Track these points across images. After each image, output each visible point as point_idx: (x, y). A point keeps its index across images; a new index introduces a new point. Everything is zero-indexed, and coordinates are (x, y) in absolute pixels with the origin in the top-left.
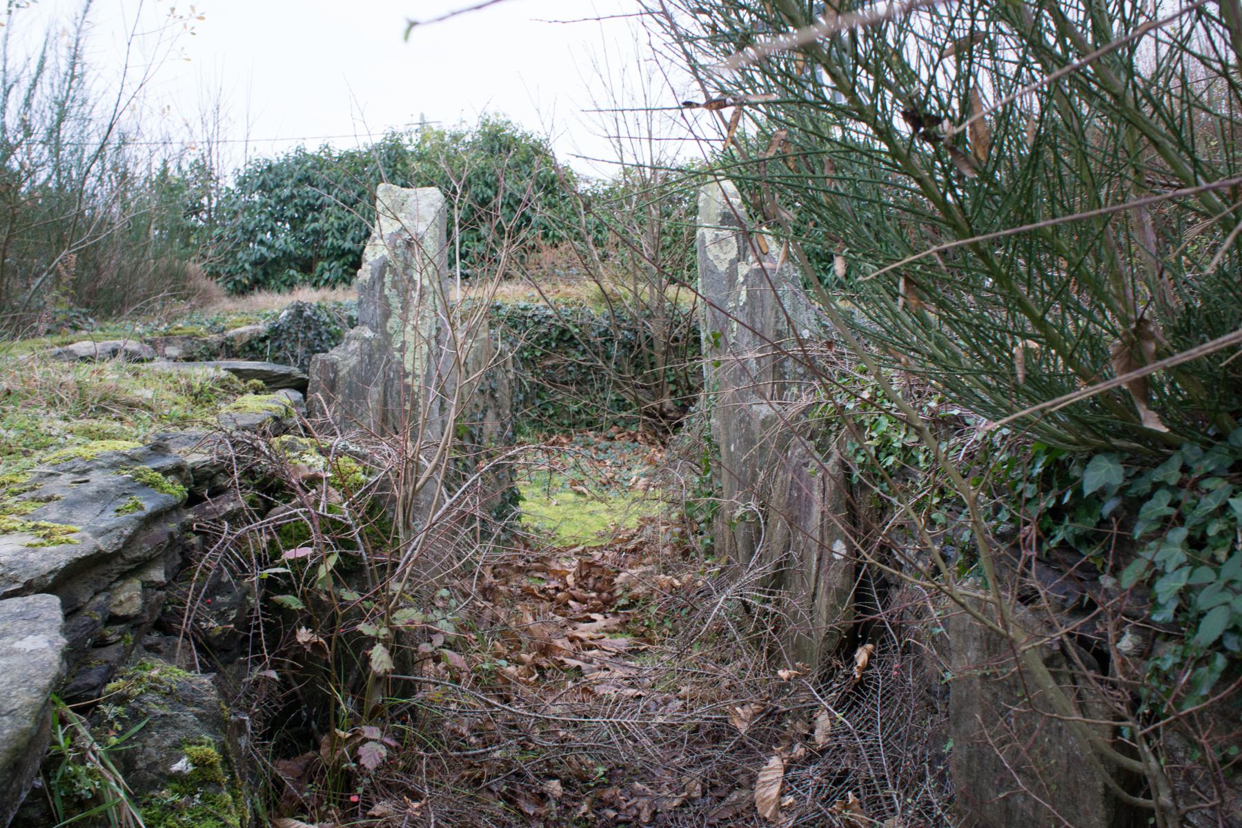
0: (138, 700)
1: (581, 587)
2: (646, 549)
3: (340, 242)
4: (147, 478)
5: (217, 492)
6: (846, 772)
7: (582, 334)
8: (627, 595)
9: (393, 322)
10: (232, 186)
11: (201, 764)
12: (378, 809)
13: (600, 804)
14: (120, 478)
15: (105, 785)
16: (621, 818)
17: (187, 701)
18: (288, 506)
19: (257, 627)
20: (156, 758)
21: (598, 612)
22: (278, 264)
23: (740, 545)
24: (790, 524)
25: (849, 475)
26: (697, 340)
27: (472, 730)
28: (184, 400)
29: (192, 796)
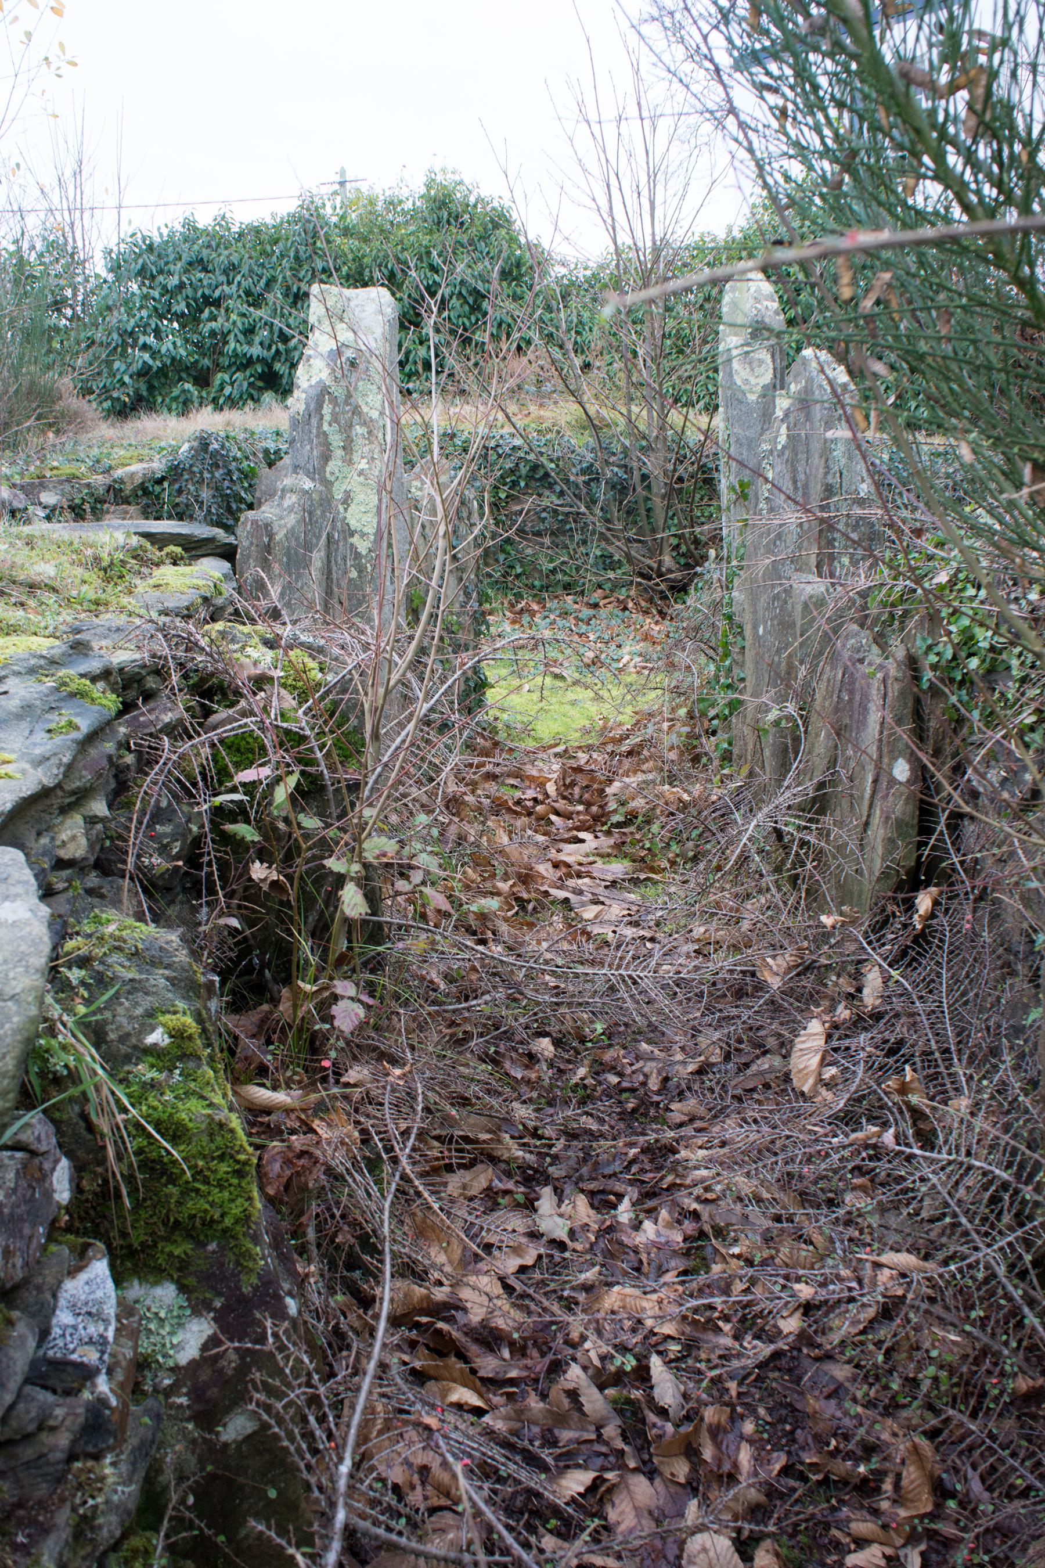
0: (102, 963)
1: (564, 798)
2: (646, 752)
3: (246, 348)
4: (73, 687)
5: (149, 696)
6: (901, 1043)
7: (559, 471)
8: (622, 810)
9: (332, 466)
10: (104, 274)
11: (178, 1035)
12: (352, 1075)
13: (599, 1068)
14: (42, 688)
15: (79, 1059)
16: (625, 1084)
17: (155, 963)
18: (231, 711)
19: (209, 864)
20: (128, 1028)
21: (587, 830)
22: (166, 376)
23: (767, 753)
24: (838, 734)
25: (917, 678)
26: (710, 483)
27: (448, 978)
28: (94, 577)
29: (171, 1071)
